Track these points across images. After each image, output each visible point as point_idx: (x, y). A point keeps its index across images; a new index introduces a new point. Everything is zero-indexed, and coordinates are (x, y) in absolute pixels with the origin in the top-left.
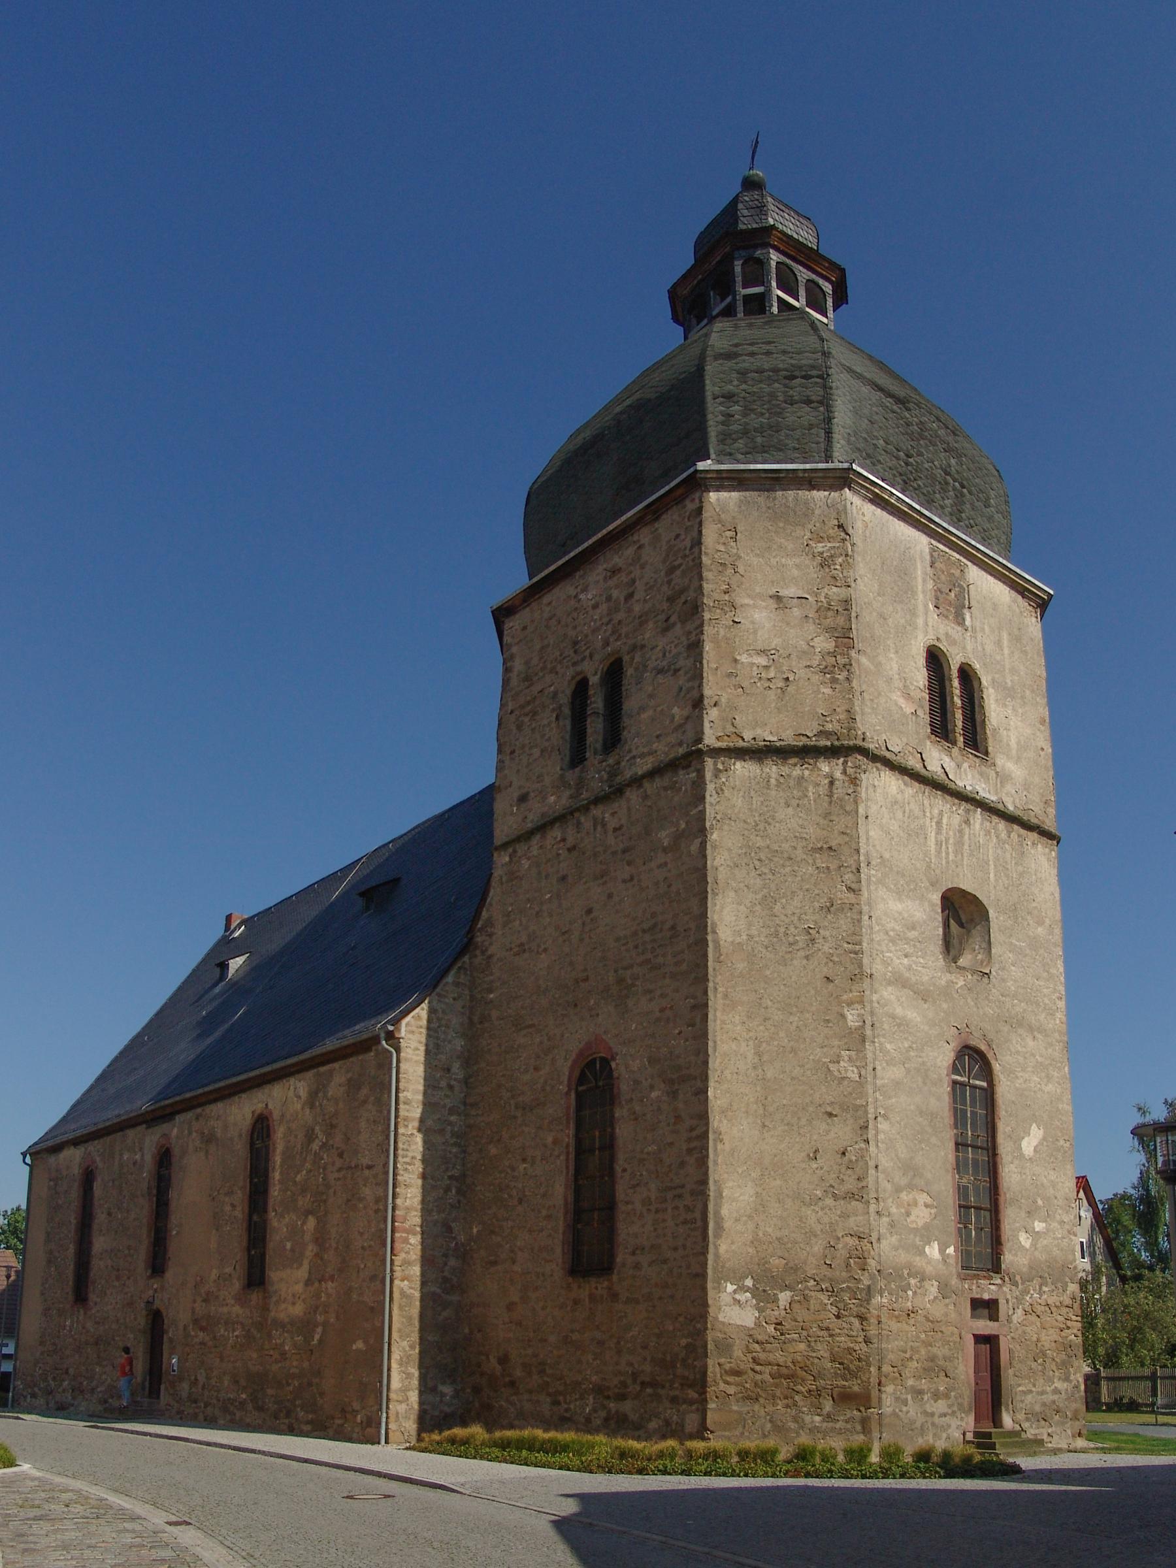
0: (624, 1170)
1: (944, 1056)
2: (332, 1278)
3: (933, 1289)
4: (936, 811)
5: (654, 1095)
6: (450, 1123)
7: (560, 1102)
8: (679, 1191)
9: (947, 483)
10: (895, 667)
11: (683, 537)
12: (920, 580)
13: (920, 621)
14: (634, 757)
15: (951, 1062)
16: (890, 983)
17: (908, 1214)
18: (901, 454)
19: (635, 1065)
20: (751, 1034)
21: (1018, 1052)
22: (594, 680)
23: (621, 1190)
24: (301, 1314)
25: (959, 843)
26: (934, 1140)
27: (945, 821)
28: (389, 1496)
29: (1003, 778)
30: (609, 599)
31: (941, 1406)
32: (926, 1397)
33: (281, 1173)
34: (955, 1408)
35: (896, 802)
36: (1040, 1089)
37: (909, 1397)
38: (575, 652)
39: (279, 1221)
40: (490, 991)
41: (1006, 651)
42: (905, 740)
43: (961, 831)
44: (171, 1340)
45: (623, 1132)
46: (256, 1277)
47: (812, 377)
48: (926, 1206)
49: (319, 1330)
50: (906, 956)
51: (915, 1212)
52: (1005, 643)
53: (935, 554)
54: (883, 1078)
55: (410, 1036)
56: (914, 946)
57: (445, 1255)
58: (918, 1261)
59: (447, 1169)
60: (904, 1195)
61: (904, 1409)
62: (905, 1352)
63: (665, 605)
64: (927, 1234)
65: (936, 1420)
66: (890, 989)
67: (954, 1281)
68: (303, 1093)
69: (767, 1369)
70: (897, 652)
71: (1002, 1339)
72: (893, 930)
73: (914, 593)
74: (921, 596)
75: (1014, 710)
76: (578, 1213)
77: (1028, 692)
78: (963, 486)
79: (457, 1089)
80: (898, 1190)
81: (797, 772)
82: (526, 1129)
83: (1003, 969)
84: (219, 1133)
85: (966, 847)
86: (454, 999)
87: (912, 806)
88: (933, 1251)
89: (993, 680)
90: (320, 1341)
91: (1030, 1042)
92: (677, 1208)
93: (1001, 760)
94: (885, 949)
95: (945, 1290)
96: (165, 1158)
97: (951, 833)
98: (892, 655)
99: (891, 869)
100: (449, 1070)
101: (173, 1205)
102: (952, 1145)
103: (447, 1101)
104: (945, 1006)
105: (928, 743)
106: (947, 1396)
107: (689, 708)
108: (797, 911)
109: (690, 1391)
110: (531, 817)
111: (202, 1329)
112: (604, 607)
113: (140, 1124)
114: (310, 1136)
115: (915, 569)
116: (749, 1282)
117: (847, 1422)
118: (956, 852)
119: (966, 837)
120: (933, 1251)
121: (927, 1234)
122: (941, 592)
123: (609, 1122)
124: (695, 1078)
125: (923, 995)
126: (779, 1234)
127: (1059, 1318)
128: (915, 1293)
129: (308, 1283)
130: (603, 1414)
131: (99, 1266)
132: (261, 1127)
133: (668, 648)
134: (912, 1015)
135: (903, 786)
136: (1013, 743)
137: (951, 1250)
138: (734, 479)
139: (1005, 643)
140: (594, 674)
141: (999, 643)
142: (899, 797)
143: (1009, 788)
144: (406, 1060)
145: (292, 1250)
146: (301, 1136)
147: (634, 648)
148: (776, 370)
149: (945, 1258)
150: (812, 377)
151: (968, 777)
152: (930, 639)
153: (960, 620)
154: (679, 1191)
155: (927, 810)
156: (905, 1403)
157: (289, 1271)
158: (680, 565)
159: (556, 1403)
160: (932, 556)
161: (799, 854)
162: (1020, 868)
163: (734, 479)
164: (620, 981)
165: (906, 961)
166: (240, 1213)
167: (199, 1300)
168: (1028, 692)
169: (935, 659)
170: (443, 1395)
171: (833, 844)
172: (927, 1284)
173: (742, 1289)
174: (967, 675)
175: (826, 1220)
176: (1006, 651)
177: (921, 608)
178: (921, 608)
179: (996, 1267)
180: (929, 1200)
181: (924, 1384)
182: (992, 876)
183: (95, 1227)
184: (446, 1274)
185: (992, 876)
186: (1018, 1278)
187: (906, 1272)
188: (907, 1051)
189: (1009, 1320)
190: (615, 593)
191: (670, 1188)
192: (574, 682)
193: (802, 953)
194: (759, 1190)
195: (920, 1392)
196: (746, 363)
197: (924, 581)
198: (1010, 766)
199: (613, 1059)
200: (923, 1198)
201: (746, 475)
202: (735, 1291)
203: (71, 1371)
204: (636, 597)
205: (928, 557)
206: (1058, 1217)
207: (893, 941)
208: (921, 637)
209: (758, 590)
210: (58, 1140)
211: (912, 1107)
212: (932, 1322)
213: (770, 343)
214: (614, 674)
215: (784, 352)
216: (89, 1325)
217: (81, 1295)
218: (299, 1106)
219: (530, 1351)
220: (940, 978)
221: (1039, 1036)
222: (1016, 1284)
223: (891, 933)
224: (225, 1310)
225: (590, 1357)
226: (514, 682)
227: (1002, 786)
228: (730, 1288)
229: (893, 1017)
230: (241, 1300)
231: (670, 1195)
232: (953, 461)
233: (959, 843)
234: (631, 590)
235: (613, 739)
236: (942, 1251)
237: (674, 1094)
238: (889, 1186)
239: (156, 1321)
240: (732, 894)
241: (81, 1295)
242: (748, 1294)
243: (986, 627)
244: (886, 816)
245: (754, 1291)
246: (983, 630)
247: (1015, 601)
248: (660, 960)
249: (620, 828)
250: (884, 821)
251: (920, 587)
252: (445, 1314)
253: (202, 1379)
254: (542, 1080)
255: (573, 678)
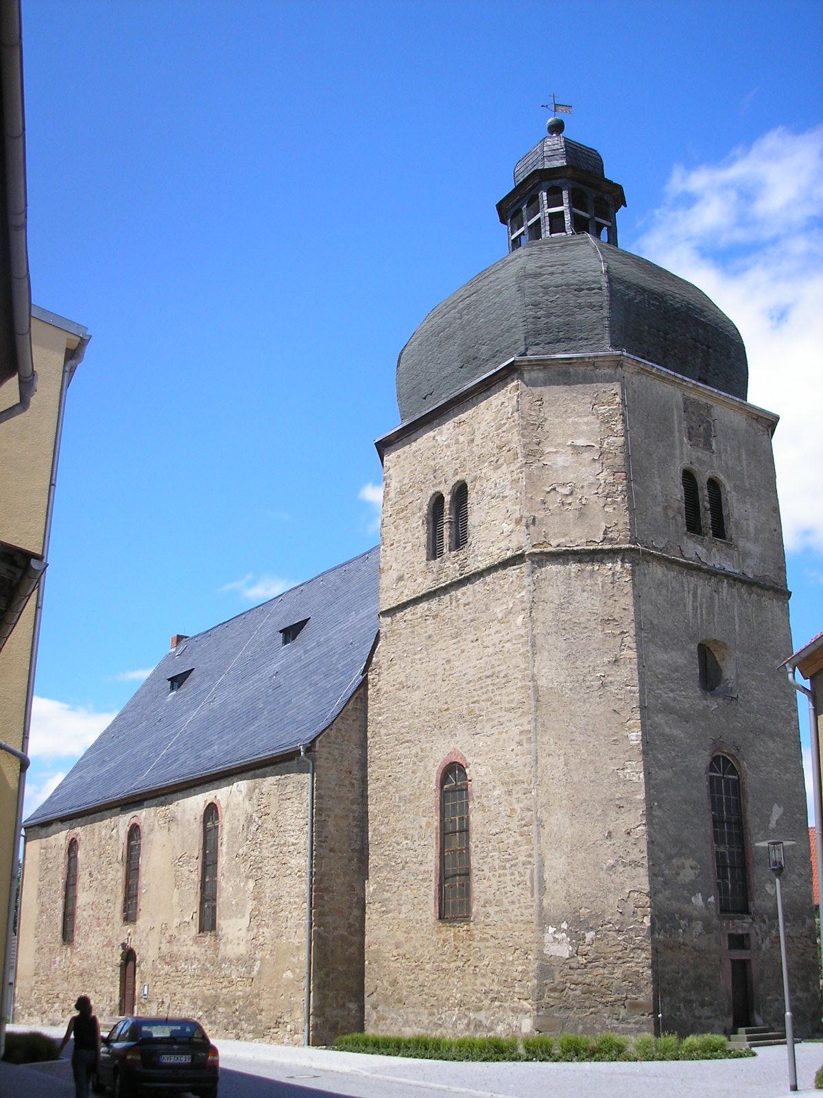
0: (477, 846)
1: (702, 760)
2: (267, 926)
3: (698, 927)
4: (692, 585)
5: (496, 793)
6: (353, 811)
7: (431, 798)
8: (514, 862)
9: (696, 348)
10: (659, 487)
11: (506, 404)
12: (676, 422)
13: (677, 452)
14: (476, 556)
15: (708, 764)
16: (659, 711)
17: (678, 874)
18: (661, 333)
19: (482, 770)
20: (561, 751)
21: (761, 753)
22: (447, 498)
23: (474, 861)
24: (245, 952)
25: (711, 606)
26: (696, 821)
27: (699, 591)
28: (317, 1077)
29: (746, 555)
30: (457, 442)
31: (706, 1011)
32: (694, 1005)
33: (228, 848)
34: (718, 1013)
35: (661, 583)
36: (780, 778)
37: (682, 1006)
38: (435, 477)
39: (227, 883)
40: (380, 715)
41: (744, 463)
42: (667, 539)
43: (712, 598)
44: (142, 972)
45: (475, 818)
46: (208, 923)
47: (594, 289)
48: (692, 868)
49: (258, 963)
50: (672, 691)
51: (682, 873)
52: (744, 456)
53: (688, 402)
54: (656, 779)
55: (322, 749)
56: (678, 683)
57: (350, 907)
58: (687, 908)
59: (350, 844)
60: (674, 861)
61: (678, 1014)
62: (678, 973)
63: (496, 451)
64: (692, 888)
65: (703, 1021)
66: (660, 716)
67: (715, 921)
68: (244, 790)
69: (580, 987)
70: (660, 477)
71: (753, 964)
72: (662, 673)
73: (672, 433)
74: (677, 434)
75: (752, 504)
76: (443, 876)
77: (762, 491)
78: (709, 347)
79: (356, 786)
80: (670, 858)
81: (589, 568)
82: (407, 815)
83: (747, 693)
84: (179, 816)
85: (716, 608)
86: (353, 721)
87: (674, 584)
88: (698, 900)
89: (735, 486)
90: (259, 972)
91: (771, 744)
92: (512, 874)
93: (741, 543)
94: (655, 688)
95: (708, 928)
96: (134, 831)
97: (704, 600)
98: (656, 480)
99: (658, 631)
100: (350, 772)
101: (143, 869)
102: (710, 823)
103: (349, 795)
104: (703, 724)
105: (685, 538)
106: (711, 1004)
107: (514, 524)
108: (592, 664)
109: (525, 1003)
110: (406, 592)
111: (168, 964)
112: (454, 448)
113: (116, 807)
114: (250, 820)
115: (673, 415)
116: (564, 926)
117: (636, 1023)
118: (708, 614)
119: (716, 601)
120: (698, 900)
121: (692, 888)
122: (693, 429)
123: (465, 809)
124: (523, 782)
125: (684, 717)
126: (584, 891)
127: (800, 945)
128: (684, 931)
129: (249, 929)
130: (465, 1021)
131: (82, 915)
132: (211, 811)
133: (498, 481)
134: (677, 732)
135: (666, 572)
136: (752, 530)
137: (712, 899)
138: (540, 365)
139: (744, 456)
140: (446, 491)
141: (739, 458)
142: (664, 579)
143: (750, 562)
144: (320, 766)
145: (237, 904)
146: (242, 819)
147: (475, 479)
148: (568, 285)
149: (707, 904)
150: (594, 289)
151: (718, 559)
152: (685, 463)
153: (707, 445)
154: (514, 862)
155: (686, 586)
156: (679, 1009)
157: (234, 920)
158: (506, 424)
159: (431, 1014)
160: (685, 404)
161: (592, 624)
162: (760, 619)
163: (540, 365)
164: (471, 712)
165: (671, 695)
166: (196, 876)
167: (164, 941)
168: (762, 491)
169: (689, 477)
170: (350, 1010)
171: (615, 616)
172: (693, 924)
173: (559, 930)
174: (713, 484)
175: (618, 880)
176: (744, 463)
177: (677, 442)
178: (677, 442)
179: (745, 910)
180: (694, 863)
181: (693, 996)
182: (737, 626)
183: (79, 885)
184: (350, 921)
185: (737, 626)
186: (765, 917)
187: (677, 916)
188: (674, 758)
189: (759, 948)
190: (461, 439)
191: (508, 860)
192: (435, 497)
193: (596, 693)
194: (570, 860)
195: (691, 1002)
196: (547, 280)
197: (680, 423)
198: (750, 546)
199: (467, 767)
200: (689, 862)
201: (549, 362)
202: (555, 933)
203: (61, 996)
204: (476, 443)
205: (682, 405)
206: (797, 871)
207: (661, 682)
208: (678, 462)
209: (559, 441)
210: (49, 817)
211: (679, 799)
212: (698, 951)
213: (563, 265)
214: (461, 492)
215: (574, 272)
216: (76, 961)
217: (67, 935)
218: (241, 799)
219: (412, 977)
220: (698, 704)
221: (778, 739)
222: (764, 922)
223: (660, 676)
224: (185, 949)
225: (455, 980)
226: (392, 495)
227: (743, 561)
228: (551, 930)
229: (663, 735)
230: (196, 941)
231: (508, 865)
232: (701, 331)
233: (711, 606)
234: (472, 437)
235: (460, 541)
236: (705, 900)
237: (509, 793)
238: (662, 856)
239: (129, 956)
240: (546, 654)
241: (67, 935)
242: (564, 934)
243: (728, 448)
244: (654, 594)
245: (569, 933)
246: (726, 450)
247: (750, 426)
248: (498, 698)
249: (468, 604)
250: (653, 598)
251: (676, 428)
252: (350, 950)
253: (167, 1001)
254: (417, 780)
255: (434, 495)
